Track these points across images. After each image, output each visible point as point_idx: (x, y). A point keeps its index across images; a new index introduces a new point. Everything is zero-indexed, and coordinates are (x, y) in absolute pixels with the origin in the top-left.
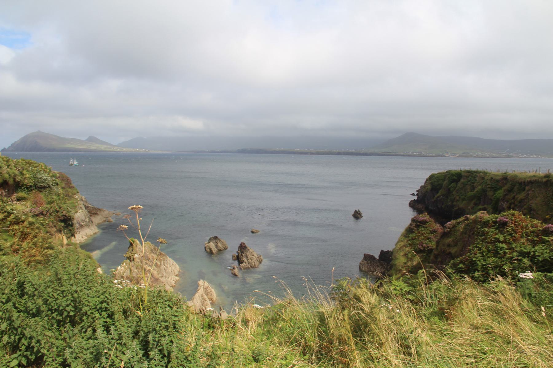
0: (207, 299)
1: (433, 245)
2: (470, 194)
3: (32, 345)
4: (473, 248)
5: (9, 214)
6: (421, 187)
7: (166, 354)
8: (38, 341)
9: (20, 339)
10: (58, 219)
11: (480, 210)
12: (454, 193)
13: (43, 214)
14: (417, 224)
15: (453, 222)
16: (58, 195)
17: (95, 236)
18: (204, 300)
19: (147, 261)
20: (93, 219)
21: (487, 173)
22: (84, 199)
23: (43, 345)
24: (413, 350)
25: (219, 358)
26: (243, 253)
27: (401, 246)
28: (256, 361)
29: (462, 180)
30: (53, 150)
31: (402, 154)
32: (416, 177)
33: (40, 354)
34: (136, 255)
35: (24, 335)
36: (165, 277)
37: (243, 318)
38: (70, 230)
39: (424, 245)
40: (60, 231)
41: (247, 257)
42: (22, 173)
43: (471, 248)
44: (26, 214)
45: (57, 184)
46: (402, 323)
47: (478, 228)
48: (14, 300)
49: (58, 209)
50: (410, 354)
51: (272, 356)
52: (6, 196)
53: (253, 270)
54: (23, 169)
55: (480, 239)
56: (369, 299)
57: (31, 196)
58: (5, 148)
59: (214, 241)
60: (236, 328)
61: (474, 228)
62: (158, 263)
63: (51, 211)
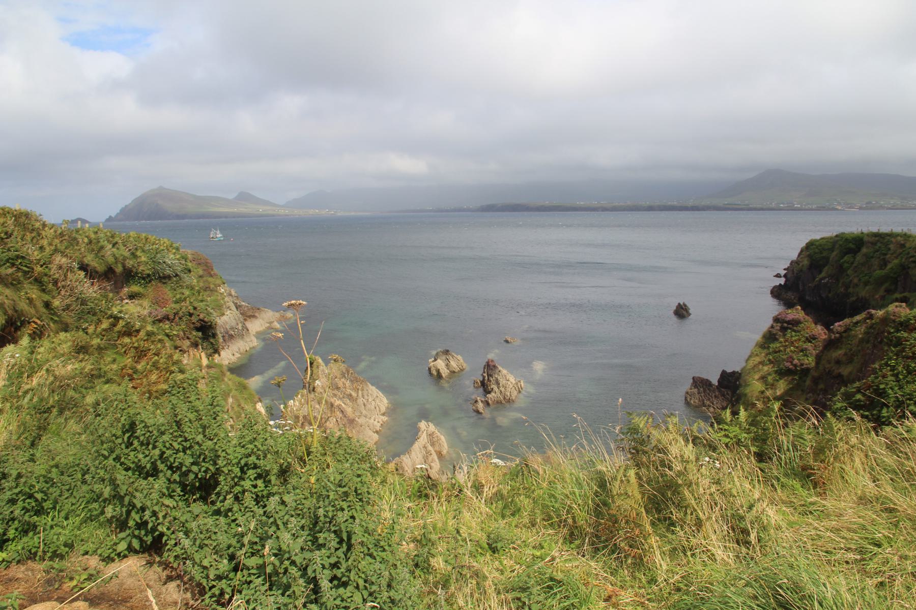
0: (433, 452)
1: (810, 361)
2: (879, 273)
3: (145, 518)
4: (880, 366)
5: (117, 319)
6: (792, 262)
7: (345, 538)
8: (154, 514)
9: (128, 513)
10: (192, 326)
11: (897, 300)
12: (849, 272)
13: (168, 319)
14: (783, 325)
15: (847, 321)
16: (192, 288)
17: (253, 351)
18: (428, 453)
19: (336, 392)
20: (249, 325)
21: (910, 236)
22: (233, 293)
23: (161, 520)
24: (753, 537)
25: (433, 544)
26: (491, 376)
27: (756, 362)
28: (494, 550)
29: (864, 250)
30: (183, 217)
31: (759, 206)
32: (782, 245)
33: (157, 533)
34: (317, 382)
35: (134, 506)
36: (366, 417)
37: (474, 482)
38: (212, 343)
39: (796, 361)
40: (195, 345)
41: (498, 383)
42: (134, 255)
43: (877, 366)
44: (143, 319)
45: (190, 271)
46: (734, 492)
47: (889, 333)
48: (118, 452)
49: (191, 311)
50: (747, 543)
51: (519, 542)
52: (111, 291)
53: (508, 405)
54: (136, 249)
55: (892, 352)
56: (680, 449)
57: (150, 291)
58: (110, 217)
59: (444, 358)
60: (462, 496)
61: (884, 332)
62: (354, 394)
63: (181, 314)
